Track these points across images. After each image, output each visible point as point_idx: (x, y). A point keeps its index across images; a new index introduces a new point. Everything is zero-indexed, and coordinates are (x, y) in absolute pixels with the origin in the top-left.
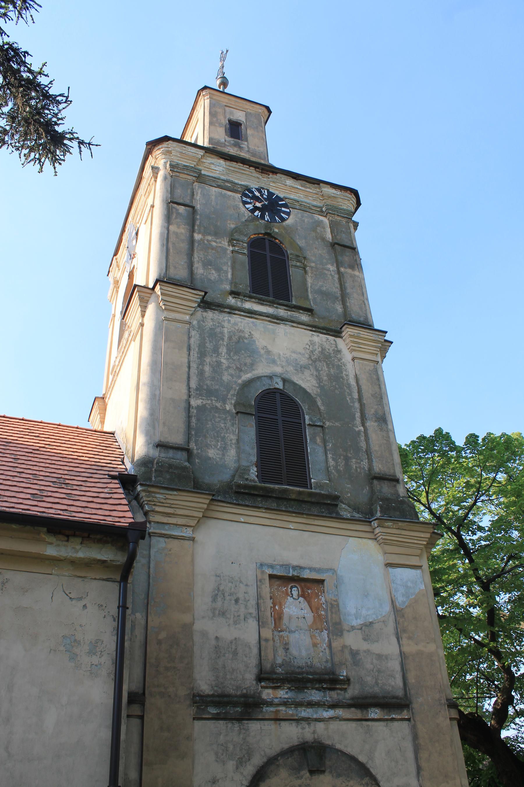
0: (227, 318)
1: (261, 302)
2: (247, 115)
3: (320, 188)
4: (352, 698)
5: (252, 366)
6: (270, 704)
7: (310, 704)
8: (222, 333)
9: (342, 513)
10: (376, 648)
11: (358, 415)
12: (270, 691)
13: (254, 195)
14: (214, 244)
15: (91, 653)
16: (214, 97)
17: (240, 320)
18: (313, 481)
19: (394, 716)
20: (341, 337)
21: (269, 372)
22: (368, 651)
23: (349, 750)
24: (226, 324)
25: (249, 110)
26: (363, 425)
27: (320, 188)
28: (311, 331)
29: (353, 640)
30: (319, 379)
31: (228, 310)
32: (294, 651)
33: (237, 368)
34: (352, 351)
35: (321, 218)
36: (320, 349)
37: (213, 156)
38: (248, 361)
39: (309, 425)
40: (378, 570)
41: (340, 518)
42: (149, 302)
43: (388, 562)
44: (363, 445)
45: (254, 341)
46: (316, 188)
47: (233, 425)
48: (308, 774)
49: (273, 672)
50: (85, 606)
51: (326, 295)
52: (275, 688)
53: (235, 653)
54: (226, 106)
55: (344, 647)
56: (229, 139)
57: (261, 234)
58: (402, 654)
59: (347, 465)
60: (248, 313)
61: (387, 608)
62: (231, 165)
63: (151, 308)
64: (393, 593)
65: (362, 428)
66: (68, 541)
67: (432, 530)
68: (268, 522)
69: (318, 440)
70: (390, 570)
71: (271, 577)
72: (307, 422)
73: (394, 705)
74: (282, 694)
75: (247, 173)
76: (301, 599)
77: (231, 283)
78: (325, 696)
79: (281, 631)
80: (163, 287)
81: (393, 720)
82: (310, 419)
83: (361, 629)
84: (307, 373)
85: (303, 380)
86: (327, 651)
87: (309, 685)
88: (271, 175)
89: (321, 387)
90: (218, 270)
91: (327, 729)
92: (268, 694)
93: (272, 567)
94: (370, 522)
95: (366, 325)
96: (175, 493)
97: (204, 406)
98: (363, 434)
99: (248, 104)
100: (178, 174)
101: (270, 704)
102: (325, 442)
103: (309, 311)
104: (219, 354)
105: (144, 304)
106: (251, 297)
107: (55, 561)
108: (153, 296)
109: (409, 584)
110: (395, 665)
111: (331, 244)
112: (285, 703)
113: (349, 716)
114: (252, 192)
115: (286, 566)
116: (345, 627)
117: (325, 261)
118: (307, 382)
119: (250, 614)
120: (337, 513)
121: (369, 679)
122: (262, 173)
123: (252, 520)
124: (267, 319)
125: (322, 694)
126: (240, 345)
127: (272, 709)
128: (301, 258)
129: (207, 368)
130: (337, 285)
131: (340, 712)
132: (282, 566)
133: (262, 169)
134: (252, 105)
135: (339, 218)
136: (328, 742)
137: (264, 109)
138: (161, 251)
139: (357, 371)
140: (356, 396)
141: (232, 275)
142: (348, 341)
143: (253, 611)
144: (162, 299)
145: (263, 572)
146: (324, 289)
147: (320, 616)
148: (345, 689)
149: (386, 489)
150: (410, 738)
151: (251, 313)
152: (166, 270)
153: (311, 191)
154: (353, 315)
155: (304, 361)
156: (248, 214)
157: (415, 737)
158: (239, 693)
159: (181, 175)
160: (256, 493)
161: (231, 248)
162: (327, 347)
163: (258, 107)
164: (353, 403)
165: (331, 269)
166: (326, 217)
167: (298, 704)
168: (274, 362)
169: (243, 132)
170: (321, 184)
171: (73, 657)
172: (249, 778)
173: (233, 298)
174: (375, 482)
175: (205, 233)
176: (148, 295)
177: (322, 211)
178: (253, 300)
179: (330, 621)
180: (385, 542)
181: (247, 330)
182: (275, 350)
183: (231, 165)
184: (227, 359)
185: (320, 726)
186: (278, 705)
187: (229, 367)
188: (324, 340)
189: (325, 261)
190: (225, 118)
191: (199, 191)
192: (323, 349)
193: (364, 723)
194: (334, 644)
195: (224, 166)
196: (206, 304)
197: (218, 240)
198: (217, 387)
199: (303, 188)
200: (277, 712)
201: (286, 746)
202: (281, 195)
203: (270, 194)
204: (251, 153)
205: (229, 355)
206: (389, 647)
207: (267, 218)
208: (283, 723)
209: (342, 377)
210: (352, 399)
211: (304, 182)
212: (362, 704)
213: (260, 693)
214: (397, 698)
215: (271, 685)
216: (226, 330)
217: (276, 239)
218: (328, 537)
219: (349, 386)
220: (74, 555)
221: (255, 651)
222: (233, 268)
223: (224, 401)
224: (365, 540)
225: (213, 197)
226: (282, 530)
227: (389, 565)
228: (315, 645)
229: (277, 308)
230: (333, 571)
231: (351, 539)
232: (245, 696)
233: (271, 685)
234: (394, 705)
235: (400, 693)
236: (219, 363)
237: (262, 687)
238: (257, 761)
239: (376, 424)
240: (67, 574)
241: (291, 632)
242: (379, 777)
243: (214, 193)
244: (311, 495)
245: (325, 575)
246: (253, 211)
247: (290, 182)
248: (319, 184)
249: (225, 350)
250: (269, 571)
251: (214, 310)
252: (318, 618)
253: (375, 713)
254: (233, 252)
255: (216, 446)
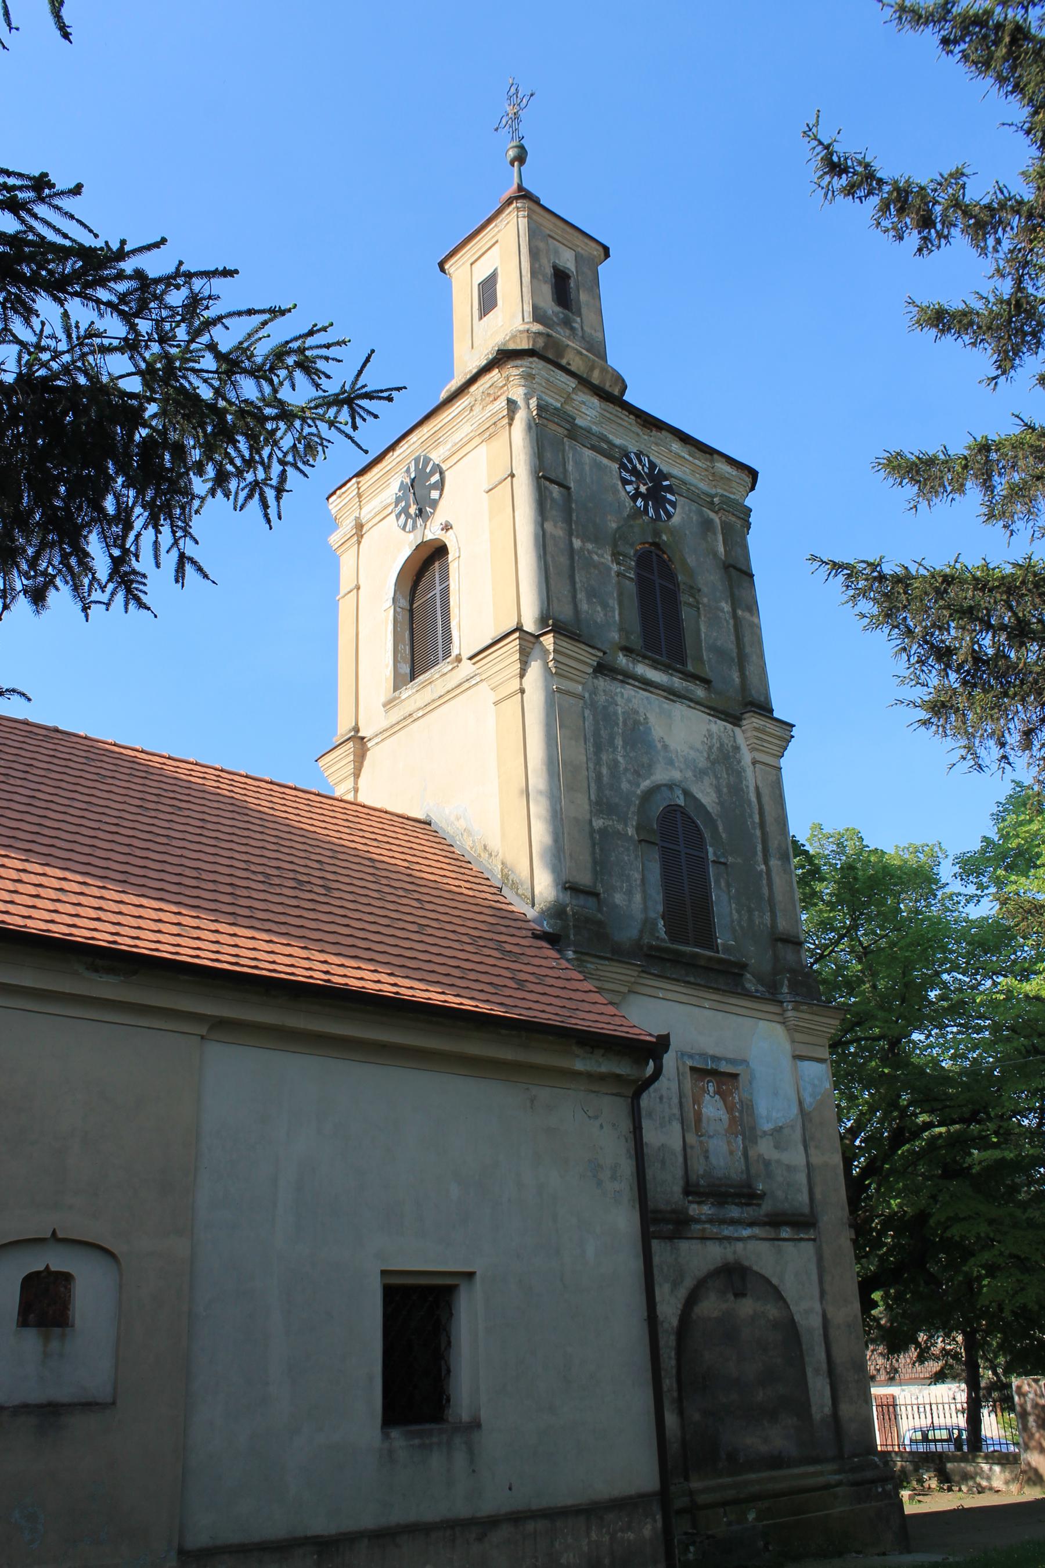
0: (618, 690)
1: (656, 665)
2: (578, 258)
3: (712, 461)
4: (767, 1215)
5: (650, 767)
6: (698, 1221)
7: (733, 1222)
8: (616, 713)
9: (748, 985)
10: (786, 1157)
11: (759, 847)
12: (695, 1206)
13: (634, 467)
14: (595, 557)
15: (613, 1178)
16: (534, 217)
17: (633, 693)
18: (719, 941)
19: (802, 1236)
20: (740, 726)
21: (668, 778)
22: (778, 1161)
23: (763, 1272)
24: (619, 699)
25: (579, 249)
26: (766, 862)
27: (712, 461)
28: (709, 714)
29: (765, 1148)
30: (718, 790)
31: (620, 677)
32: (713, 1160)
33: (635, 770)
34: (753, 750)
35: (712, 515)
36: (718, 745)
37: (586, 390)
38: (645, 760)
39: (714, 862)
40: (786, 1062)
41: (747, 995)
42: (531, 657)
43: (797, 1053)
44: (765, 891)
45: (650, 729)
46: (706, 460)
47: (636, 857)
48: (732, 1298)
49: (698, 1185)
50: (601, 1126)
51: (720, 652)
52: (699, 1203)
53: (663, 1162)
54: (550, 236)
55: (760, 1156)
56: (558, 309)
57: (647, 543)
58: (808, 1164)
59: (751, 920)
60: (643, 683)
61: (795, 1110)
62: (607, 408)
63: (535, 668)
64: (801, 1091)
65: (763, 867)
66: (592, 1053)
67: (842, 1017)
68: (683, 998)
69: (723, 884)
70: (799, 1063)
71: (693, 1069)
72: (711, 857)
73: (803, 1222)
74: (707, 1210)
75: (625, 424)
76: (717, 1097)
77: (621, 630)
78: (742, 1213)
79: (701, 1136)
80: (558, 642)
81: (801, 1239)
82: (715, 854)
83: (772, 1135)
84: (707, 781)
85: (702, 792)
86: (742, 1160)
87: (730, 1200)
88: (654, 433)
89: (721, 803)
90: (605, 606)
91: (745, 1249)
92: (694, 1210)
93: (691, 1056)
94: (782, 1002)
95: (764, 709)
96: (607, 962)
97: (606, 828)
98: (765, 876)
99: (581, 237)
100: (545, 422)
101: (698, 1221)
102: (728, 885)
103: (706, 682)
104: (615, 749)
105: (524, 659)
106: (645, 657)
107: (574, 1075)
108: (537, 648)
109: (816, 1082)
110: (802, 1178)
111: (724, 563)
112: (711, 1221)
113: (763, 1235)
114: (630, 461)
115: (703, 1056)
116: (759, 1133)
117: (718, 594)
118: (706, 795)
119: (674, 1115)
120: (744, 988)
121: (780, 1194)
122: (643, 426)
123: (669, 995)
124: (662, 693)
125: (740, 1210)
126: (637, 735)
127: (699, 1227)
128: (694, 591)
129: (605, 771)
130: (733, 638)
131: (756, 1231)
132: (700, 1055)
133: (645, 421)
134: (586, 240)
135: (734, 519)
136: (746, 1263)
137: (601, 249)
138: (539, 568)
139: (759, 783)
140: (757, 819)
141: (620, 614)
142: (749, 734)
143: (676, 1111)
144: (554, 659)
145: (684, 1063)
146: (719, 643)
147: (734, 1117)
148: (759, 1205)
149: (788, 954)
150: (814, 1260)
151: (647, 684)
152: (548, 605)
153: (700, 464)
154: (753, 692)
155: (702, 763)
156: (629, 503)
157: (820, 1259)
158: (669, 1208)
159: (551, 425)
160: (667, 957)
161: (615, 567)
162: (726, 741)
163: (593, 245)
164: (754, 828)
165: (726, 610)
166: (716, 512)
167: (723, 1222)
168: (671, 762)
169: (573, 296)
170: (715, 456)
171: (599, 1183)
172: (683, 1301)
173: (624, 656)
174: (780, 945)
175: (585, 538)
176: (531, 645)
177: (712, 503)
178: (647, 661)
179: (743, 1124)
180: (797, 1029)
181: (641, 710)
182: (673, 745)
183: (607, 408)
184: (624, 756)
185: (740, 1246)
186: (705, 1222)
187: (626, 770)
188: (722, 729)
189: (718, 594)
190: (549, 261)
191: (571, 455)
192: (722, 745)
193: (776, 1243)
194: (751, 1153)
195: (599, 410)
196: (603, 669)
197: (600, 552)
198: (617, 800)
199: (691, 459)
200: (704, 1230)
201: (712, 1267)
202: (665, 469)
203: (653, 465)
204: (588, 342)
205: (625, 751)
206: (796, 1157)
207: (651, 512)
208: (708, 1243)
209: (742, 790)
210: (753, 823)
211: (693, 449)
212: (776, 1221)
213: (687, 1209)
214: (802, 1215)
215: (698, 1199)
216: (620, 710)
217: (664, 553)
218: (740, 1019)
219: (749, 802)
220: (599, 1070)
221: (681, 1159)
222: (621, 604)
223: (624, 820)
224: (774, 1024)
225: (587, 468)
226: (697, 1009)
227: (798, 1057)
228: (731, 1153)
229: (671, 675)
230: (744, 1062)
231: (761, 1022)
232: (673, 1211)
233: (698, 1199)
234: (803, 1222)
235: (806, 1210)
236: (616, 762)
237: (689, 1202)
238: (689, 1283)
239: (779, 863)
240: (582, 1088)
241: (710, 1137)
242: (789, 1300)
243: (587, 461)
244: (721, 961)
245: (740, 1068)
246: (634, 498)
247: (676, 446)
248: (711, 454)
249: (621, 743)
250: (689, 1063)
251: (606, 675)
252: (733, 1120)
253: (786, 1232)
254: (619, 574)
255: (622, 888)
